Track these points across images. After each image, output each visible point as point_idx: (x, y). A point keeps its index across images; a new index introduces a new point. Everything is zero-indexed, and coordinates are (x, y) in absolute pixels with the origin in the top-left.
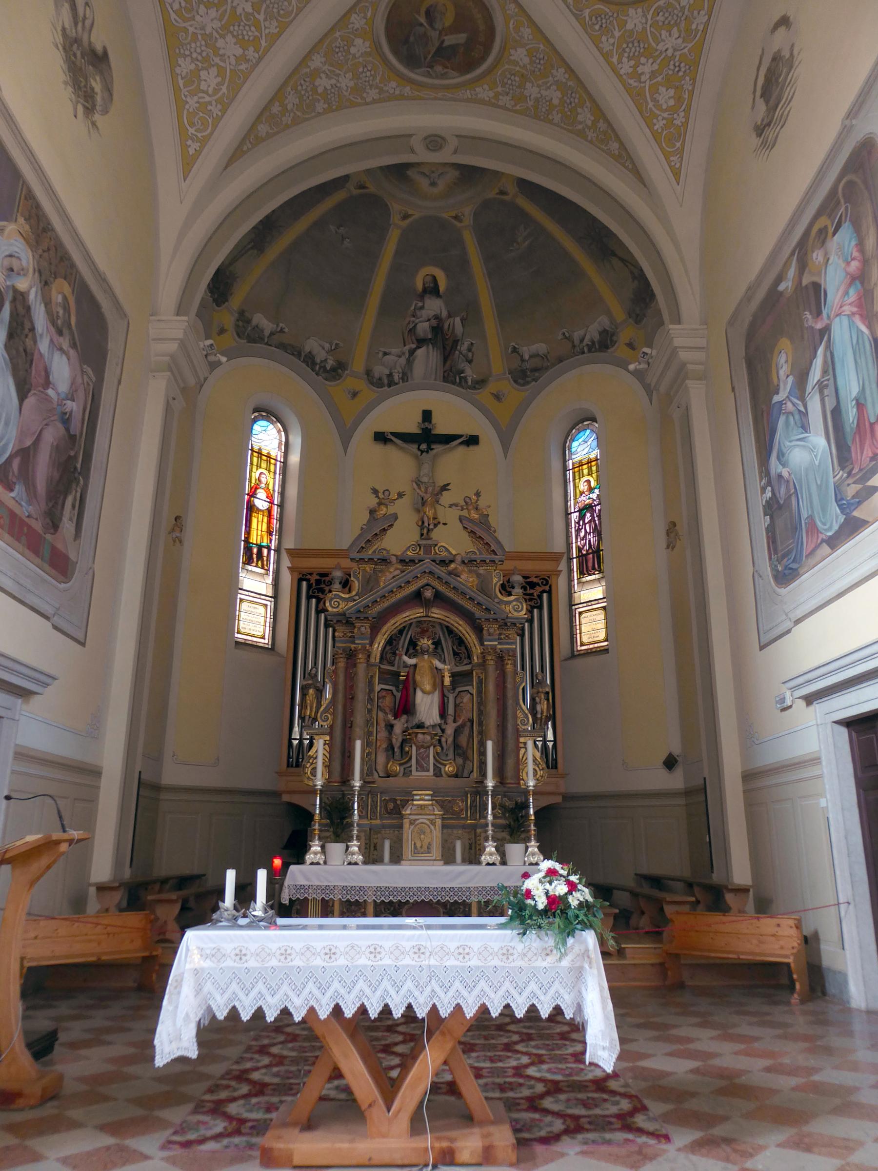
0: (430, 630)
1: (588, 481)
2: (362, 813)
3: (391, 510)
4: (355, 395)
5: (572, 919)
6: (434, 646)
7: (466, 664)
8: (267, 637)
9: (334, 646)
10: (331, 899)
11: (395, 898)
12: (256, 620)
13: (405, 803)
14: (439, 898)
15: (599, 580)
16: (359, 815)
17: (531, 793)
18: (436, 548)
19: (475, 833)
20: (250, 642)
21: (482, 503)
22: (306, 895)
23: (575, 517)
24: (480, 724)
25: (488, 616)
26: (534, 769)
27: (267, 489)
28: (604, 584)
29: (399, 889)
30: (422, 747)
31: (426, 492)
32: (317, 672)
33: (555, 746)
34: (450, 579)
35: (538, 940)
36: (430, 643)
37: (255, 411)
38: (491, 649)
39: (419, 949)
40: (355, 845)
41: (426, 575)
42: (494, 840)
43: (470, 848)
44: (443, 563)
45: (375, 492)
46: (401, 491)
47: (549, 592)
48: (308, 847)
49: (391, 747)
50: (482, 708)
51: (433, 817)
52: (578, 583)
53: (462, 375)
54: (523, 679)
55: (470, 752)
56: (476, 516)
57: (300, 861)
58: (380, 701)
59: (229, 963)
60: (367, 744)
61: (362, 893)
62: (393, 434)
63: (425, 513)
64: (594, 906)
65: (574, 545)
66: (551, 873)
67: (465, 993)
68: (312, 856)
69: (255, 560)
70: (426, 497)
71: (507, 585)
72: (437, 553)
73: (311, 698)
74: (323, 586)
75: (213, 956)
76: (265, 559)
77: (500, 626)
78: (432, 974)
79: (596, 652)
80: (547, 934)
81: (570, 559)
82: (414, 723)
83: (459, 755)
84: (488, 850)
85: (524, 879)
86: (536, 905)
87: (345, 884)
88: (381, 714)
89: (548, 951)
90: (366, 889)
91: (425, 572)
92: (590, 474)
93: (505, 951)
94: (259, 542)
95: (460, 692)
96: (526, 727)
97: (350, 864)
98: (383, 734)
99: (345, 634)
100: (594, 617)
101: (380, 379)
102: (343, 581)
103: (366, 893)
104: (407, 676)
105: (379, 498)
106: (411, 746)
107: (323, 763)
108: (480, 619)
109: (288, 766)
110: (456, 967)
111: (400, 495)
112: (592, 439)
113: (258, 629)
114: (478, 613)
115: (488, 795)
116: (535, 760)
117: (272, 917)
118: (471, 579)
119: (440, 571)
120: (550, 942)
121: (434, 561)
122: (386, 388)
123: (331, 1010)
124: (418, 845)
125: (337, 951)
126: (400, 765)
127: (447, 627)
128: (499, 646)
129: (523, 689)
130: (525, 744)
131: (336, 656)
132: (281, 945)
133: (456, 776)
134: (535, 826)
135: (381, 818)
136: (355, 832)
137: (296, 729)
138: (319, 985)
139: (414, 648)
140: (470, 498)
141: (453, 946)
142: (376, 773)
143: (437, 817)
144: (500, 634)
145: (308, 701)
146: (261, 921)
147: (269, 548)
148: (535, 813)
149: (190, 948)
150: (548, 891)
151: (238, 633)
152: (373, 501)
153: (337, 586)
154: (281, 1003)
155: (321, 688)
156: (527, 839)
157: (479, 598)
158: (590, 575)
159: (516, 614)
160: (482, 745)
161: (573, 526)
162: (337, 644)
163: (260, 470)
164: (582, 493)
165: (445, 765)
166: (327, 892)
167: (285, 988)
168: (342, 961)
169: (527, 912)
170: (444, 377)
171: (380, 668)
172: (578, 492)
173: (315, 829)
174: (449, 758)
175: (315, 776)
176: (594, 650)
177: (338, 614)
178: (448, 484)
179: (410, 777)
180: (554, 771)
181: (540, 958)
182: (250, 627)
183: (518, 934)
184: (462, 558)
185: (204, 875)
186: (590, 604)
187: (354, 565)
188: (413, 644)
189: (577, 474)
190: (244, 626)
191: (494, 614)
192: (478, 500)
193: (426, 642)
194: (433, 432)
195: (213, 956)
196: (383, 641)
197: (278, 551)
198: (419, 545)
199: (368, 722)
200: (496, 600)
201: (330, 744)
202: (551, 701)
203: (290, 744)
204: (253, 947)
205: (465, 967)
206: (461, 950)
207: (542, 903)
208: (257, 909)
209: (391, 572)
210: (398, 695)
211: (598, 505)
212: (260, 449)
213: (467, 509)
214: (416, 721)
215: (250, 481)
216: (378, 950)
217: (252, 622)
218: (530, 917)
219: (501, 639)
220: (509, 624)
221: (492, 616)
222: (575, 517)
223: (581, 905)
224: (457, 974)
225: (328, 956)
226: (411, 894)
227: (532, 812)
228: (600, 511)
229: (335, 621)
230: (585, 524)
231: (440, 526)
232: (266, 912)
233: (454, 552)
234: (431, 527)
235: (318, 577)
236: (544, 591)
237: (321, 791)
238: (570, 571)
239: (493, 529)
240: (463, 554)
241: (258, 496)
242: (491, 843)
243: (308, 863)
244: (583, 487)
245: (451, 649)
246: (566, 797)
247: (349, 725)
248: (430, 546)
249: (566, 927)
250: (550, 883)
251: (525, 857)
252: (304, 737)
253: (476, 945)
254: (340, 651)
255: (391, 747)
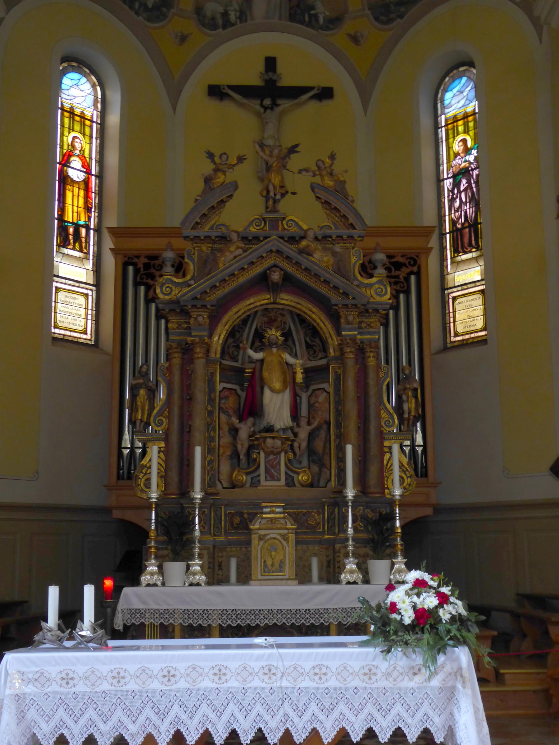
0: (279, 320)
1: (464, 141)
2: (204, 528)
3: (230, 177)
4: (183, 39)
5: (443, 634)
6: (284, 338)
7: (321, 358)
8: (89, 331)
9: (167, 339)
10: (171, 624)
11: (244, 621)
12: (76, 312)
13: (253, 516)
14: (293, 621)
15: (476, 259)
16: (201, 531)
17: (397, 503)
18: (284, 222)
19: (334, 548)
20: (70, 338)
21: (337, 168)
22: (143, 620)
23: (448, 184)
24: (338, 426)
25: (346, 302)
26: (401, 477)
27: (82, 156)
28: (482, 263)
29: (248, 612)
30: (272, 453)
31: (271, 156)
32: (148, 369)
33: (424, 451)
34: (301, 258)
35: (405, 658)
36: (278, 334)
37: (64, 60)
38: (351, 339)
39: (270, 670)
40: (197, 564)
41: (273, 254)
42: (355, 556)
43: (328, 566)
44: (293, 240)
45: (211, 156)
46: (242, 155)
47: (418, 275)
48: (143, 568)
49: (235, 455)
50: (340, 408)
51: (286, 532)
52: (452, 263)
53: (312, 12)
54: (386, 374)
55: (326, 458)
56: (331, 183)
57: (136, 582)
58: (223, 401)
59: (54, 687)
60: (208, 451)
61: (205, 617)
62: (231, 87)
63: (270, 181)
64: (468, 620)
65: (447, 218)
66: (420, 584)
67: (322, 717)
68: (148, 577)
69: (72, 241)
70: (271, 161)
71: (368, 266)
72: (285, 229)
73: (142, 400)
74: (152, 271)
75: (36, 680)
76: (83, 240)
77: (360, 313)
78: (285, 696)
79: (473, 343)
80: (414, 652)
81: (442, 235)
82: (262, 427)
83: (314, 461)
84: (348, 567)
85: (388, 592)
86: (401, 619)
87: (186, 608)
88: (223, 417)
89: (416, 670)
90: (210, 612)
91: (271, 251)
92: (466, 131)
93: (366, 671)
94: (75, 221)
95: (314, 390)
96: (391, 429)
97: (191, 585)
98: (226, 439)
99: (180, 325)
100: (470, 303)
101: (213, 19)
102: (176, 265)
103: (210, 617)
104: (253, 373)
105: (215, 163)
106: (259, 453)
107: (158, 473)
108: (336, 305)
109: (118, 478)
110: (312, 688)
111: (241, 159)
112: (469, 88)
113: (79, 323)
114: (335, 298)
115: (348, 506)
116: (401, 466)
117: (102, 636)
118: (325, 259)
119: (289, 249)
120: (418, 659)
121: (282, 238)
122: (221, 30)
123: (171, 737)
124: (269, 562)
125: (177, 673)
126: (247, 474)
127: (298, 315)
128: (359, 337)
129: (388, 385)
130: (390, 448)
131: (171, 351)
132: (112, 667)
133: (311, 485)
134: (402, 540)
135: (227, 533)
136: (197, 549)
137: (127, 436)
138: (156, 710)
139: (261, 341)
140: (323, 162)
141: (307, 666)
142: (218, 483)
143: (290, 531)
144: (361, 322)
145: (139, 403)
146: (89, 642)
147: (87, 228)
148: (402, 527)
149: (10, 672)
150: (415, 604)
151: (56, 327)
152: (208, 168)
153: (168, 269)
154: (114, 730)
155: (154, 387)
156: (392, 554)
157: (335, 280)
158: (466, 253)
159: (378, 299)
160: (341, 450)
161: (446, 195)
162: (171, 337)
163: (73, 134)
164: (456, 155)
165: (298, 474)
166: (166, 616)
167: (119, 714)
168: (182, 684)
169: (392, 627)
170: (290, 14)
171: (221, 363)
172: (452, 153)
173: (151, 547)
174: (302, 466)
175: (149, 488)
176: (470, 341)
177: (171, 302)
178: (297, 146)
179: (259, 488)
180: (424, 480)
181: (407, 678)
182: (69, 321)
183: (382, 652)
184: (315, 234)
185: (26, 602)
186: (465, 287)
187: (188, 246)
188: (259, 335)
189: (450, 132)
190: (62, 319)
191: (353, 298)
192: (332, 164)
193: (274, 334)
194: (279, 84)
195: (36, 680)
196: (224, 333)
197: (98, 230)
198: (264, 219)
199: (209, 426)
200: (356, 283)
201: (166, 452)
202: (420, 399)
203: (120, 454)
204: (81, 670)
205: (322, 688)
206: (317, 670)
207: (408, 617)
208: (85, 629)
209: (232, 252)
210: (243, 395)
211: (475, 169)
212: (72, 108)
213: (320, 175)
214: (264, 424)
215: (62, 148)
216: (223, 671)
217: (70, 314)
218: (396, 633)
219: (362, 328)
220: (370, 311)
221: (350, 302)
222: (448, 184)
223: (453, 619)
224: (312, 696)
225: (166, 679)
226: (262, 617)
227: (398, 524)
228: (478, 176)
229: (167, 310)
230: (460, 192)
231: (289, 196)
232: (94, 631)
233: (305, 227)
234: (278, 197)
235: (146, 261)
236: (411, 273)
237: (156, 504)
238: (443, 249)
239: (350, 199)
240: (316, 229)
241: (72, 165)
242: (351, 560)
243: (144, 585)
244: (457, 147)
245: (303, 340)
246: (438, 509)
247: (187, 430)
248: (277, 220)
249: (436, 643)
250: (418, 595)
251: (390, 575)
252: (136, 446)
253: (334, 665)
254: (174, 345)
255: (235, 455)
